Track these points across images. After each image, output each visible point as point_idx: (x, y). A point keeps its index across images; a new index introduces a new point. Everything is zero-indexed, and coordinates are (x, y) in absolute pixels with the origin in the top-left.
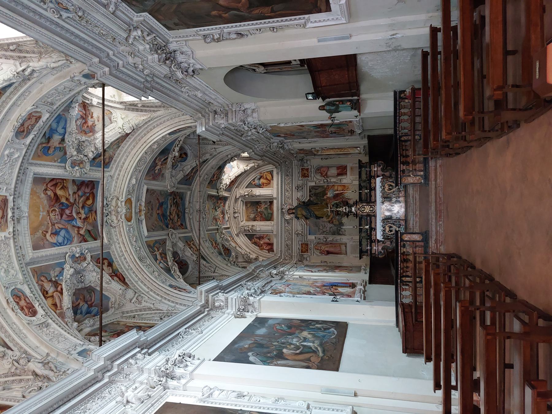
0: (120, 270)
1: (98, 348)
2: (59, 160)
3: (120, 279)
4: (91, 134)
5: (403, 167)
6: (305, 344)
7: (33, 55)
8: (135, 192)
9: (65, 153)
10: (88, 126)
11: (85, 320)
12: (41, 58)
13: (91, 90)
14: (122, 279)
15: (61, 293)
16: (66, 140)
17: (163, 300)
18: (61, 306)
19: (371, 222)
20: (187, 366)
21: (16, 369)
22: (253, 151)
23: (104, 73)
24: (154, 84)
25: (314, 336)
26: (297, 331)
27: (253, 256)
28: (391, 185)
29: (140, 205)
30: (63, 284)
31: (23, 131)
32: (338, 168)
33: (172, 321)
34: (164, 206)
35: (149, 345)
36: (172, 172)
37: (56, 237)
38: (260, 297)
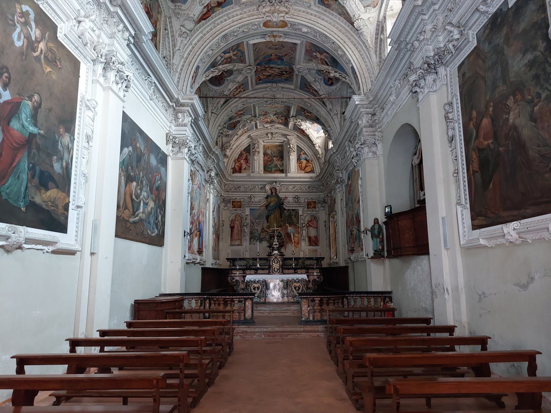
0: (214, 15)
3: (205, 14)
6: (142, 204)
14: (204, 17)
17: (183, 60)
19: (263, 269)
20: (117, 84)
24: (403, 52)
25: (150, 213)
26: (154, 197)
28: (299, 288)
29: (281, 37)
32: (316, 238)
33: (162, 69)
35: (138, 45)
36: (314, 69)
38: (188, 160)
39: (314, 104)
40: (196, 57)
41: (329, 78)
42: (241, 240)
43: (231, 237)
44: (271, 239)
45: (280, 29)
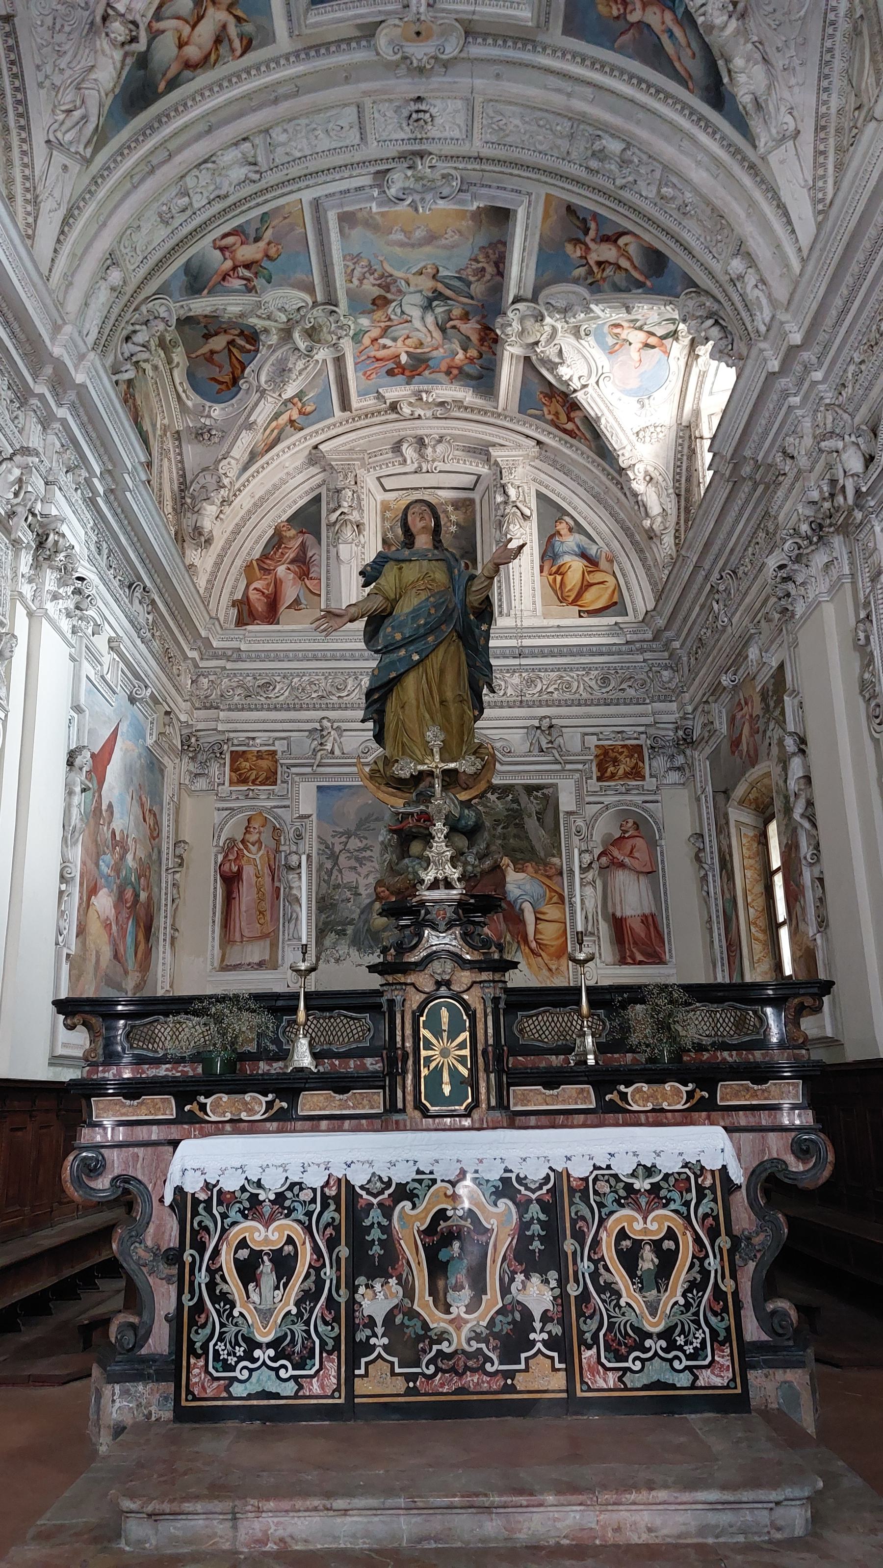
19: (340, 1084)
28: (667, 1261)
32: (650, 921)
42: (272, 938)
43: (226, 923)
44: (404, 853)
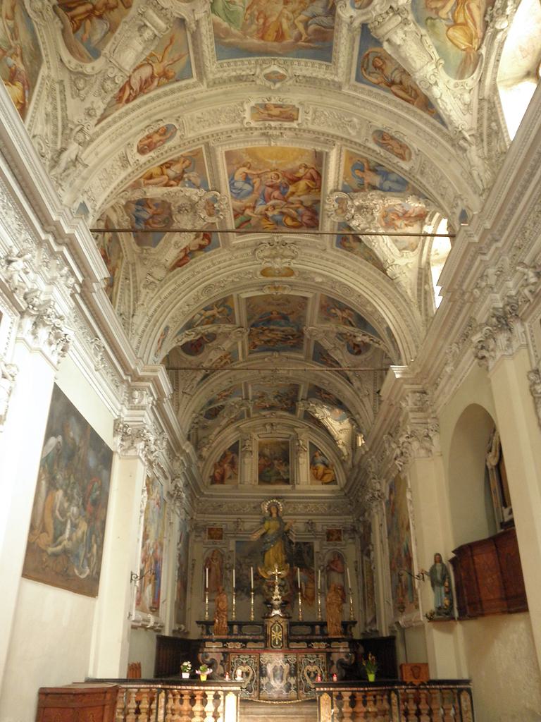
0: (193, 260)
1: (89, 228)
2: (346, 183)
3: (181, 260)
4: (383, 223)
5: (346, 696)
6: (69, 526)
7: (486, 149)
8: (303, 282)
9: (355, 191)
10: (394, 220)
11: (128, 215)
12: (483, 159)
13: (444, 222)
14: (180, 263)
15: (166, 185)
16: (373, 193)
17: (147, 318)
18: (148, 184)
20: (51, 344)
21: (72, 130)
22: (366, 452)
23: (470, 236)
24: (459, 303)
25: (80, 541)
26: (88, 515)
27: (205, 452)
28: (316, 675)
29: (285, 288)
30: (178, 188)
31: (384, 139)
33: (116, 328)
34: (283, 322)
35: (86, 296)
36: (332, 332)
37: (241, 179)
38: (144, 459)
39: (334, 381)
40: (165, 314)
41: (355, 344)
45: (284, 279)
